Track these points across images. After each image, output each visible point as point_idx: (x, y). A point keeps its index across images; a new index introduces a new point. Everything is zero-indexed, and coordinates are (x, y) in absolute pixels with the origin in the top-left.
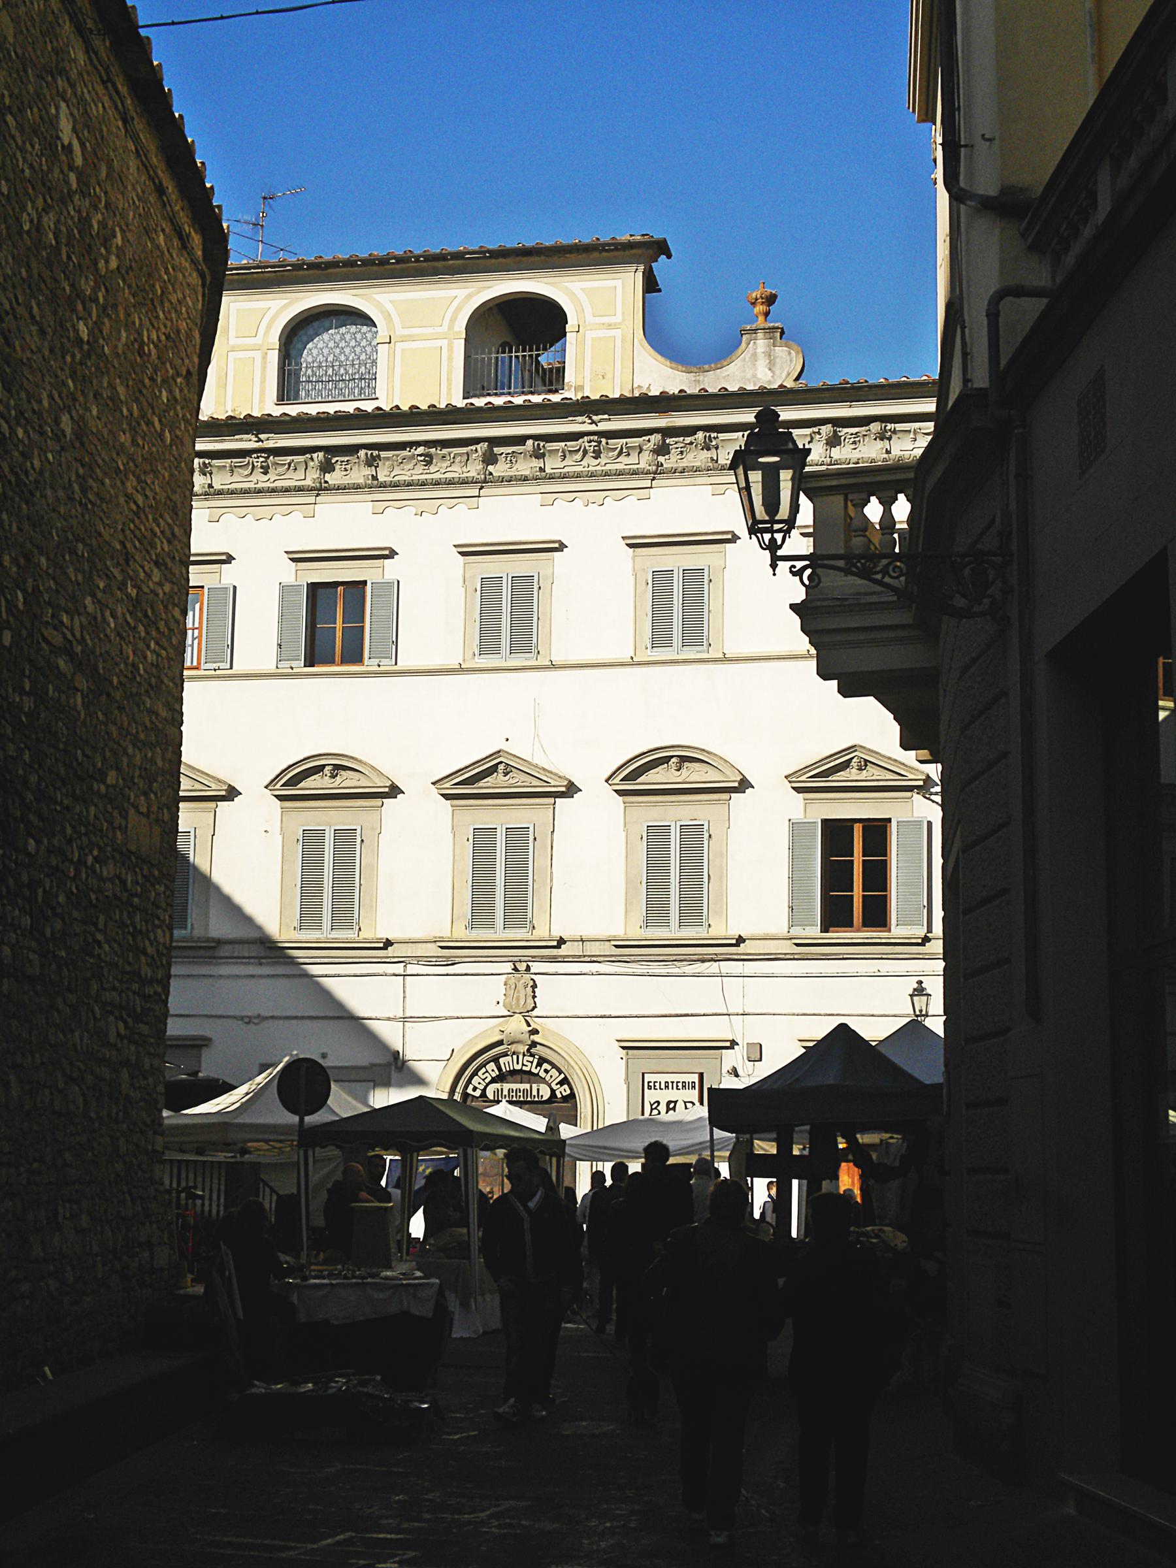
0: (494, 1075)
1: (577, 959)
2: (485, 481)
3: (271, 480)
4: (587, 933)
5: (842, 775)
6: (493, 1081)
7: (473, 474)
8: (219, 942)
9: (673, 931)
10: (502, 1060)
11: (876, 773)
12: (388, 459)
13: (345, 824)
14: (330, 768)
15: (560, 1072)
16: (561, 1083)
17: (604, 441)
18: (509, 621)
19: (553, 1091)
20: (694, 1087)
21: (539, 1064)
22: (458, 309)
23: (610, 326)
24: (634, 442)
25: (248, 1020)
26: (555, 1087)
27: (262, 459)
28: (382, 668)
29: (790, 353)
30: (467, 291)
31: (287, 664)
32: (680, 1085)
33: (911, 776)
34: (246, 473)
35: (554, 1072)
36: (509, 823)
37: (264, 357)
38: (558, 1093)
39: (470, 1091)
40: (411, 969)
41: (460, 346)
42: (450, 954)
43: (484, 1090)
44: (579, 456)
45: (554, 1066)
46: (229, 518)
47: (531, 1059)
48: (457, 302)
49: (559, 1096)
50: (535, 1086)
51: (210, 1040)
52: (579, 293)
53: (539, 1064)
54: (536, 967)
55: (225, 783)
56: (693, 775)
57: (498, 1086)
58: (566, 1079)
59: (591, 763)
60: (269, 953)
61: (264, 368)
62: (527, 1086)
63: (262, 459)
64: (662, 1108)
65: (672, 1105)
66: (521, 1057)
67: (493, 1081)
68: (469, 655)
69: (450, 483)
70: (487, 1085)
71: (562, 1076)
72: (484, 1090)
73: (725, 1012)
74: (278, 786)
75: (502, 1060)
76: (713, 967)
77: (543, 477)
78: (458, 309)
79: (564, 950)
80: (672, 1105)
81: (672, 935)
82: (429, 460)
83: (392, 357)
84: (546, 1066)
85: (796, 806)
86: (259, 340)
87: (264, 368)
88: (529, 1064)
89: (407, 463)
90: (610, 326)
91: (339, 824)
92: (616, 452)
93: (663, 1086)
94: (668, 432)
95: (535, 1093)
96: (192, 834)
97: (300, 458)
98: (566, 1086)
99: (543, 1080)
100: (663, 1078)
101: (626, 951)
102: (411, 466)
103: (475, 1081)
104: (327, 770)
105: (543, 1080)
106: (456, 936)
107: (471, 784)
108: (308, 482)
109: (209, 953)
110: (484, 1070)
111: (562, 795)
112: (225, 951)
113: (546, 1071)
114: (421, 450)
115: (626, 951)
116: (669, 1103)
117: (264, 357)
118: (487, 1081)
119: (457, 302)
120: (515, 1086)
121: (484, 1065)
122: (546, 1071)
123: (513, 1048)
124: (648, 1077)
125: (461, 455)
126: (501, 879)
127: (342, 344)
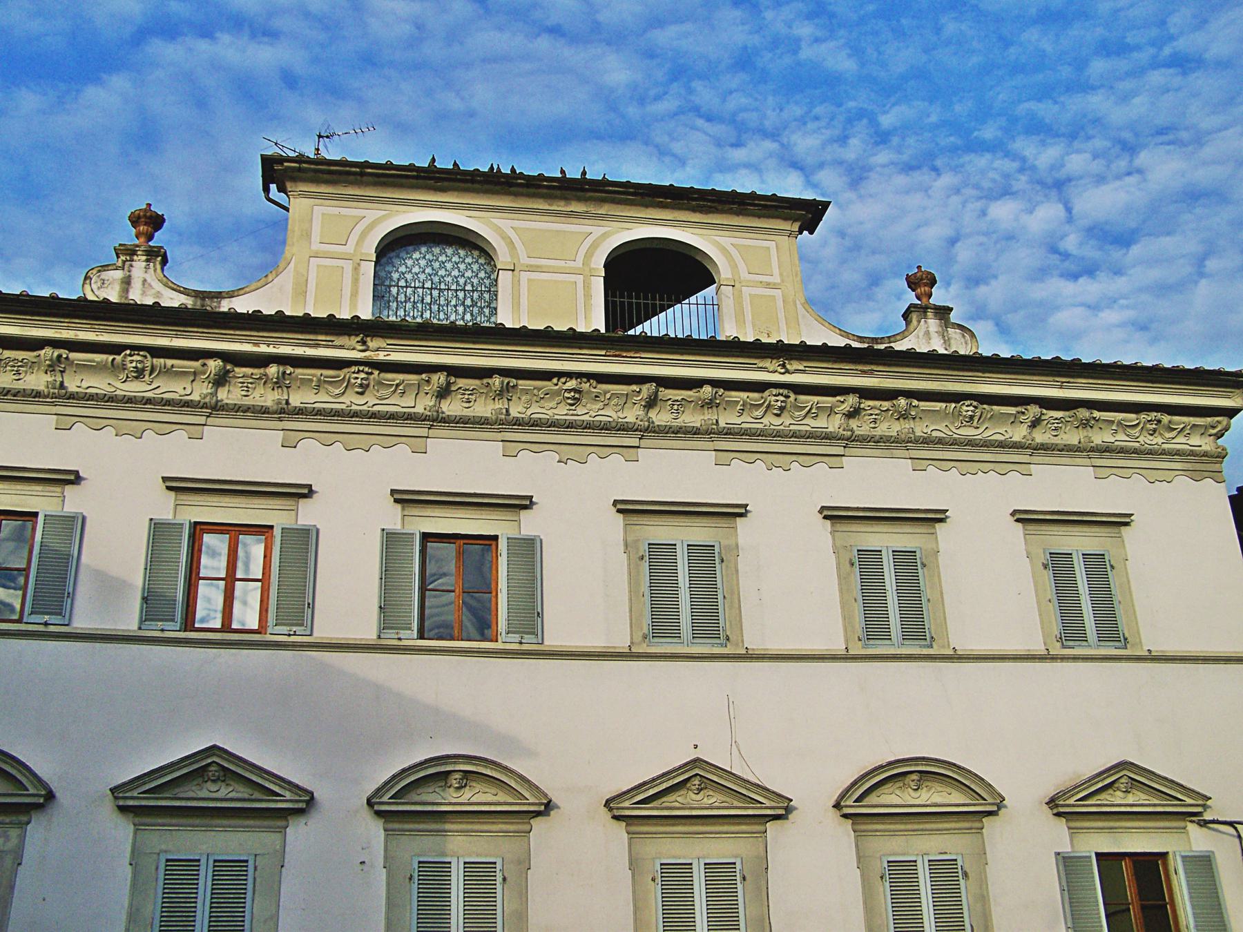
2: (646, 430)
3: (367, 402)
5: (1105, 797)
7: (631, 419)
11: (1143, 796)
12: (526, 392)
13: (674, 857)
14: (457, 776)
17: (793, 396)
23: (768, 285)
24: (828, 401)
27: (363, 375)
28: (525, 647)
30: (602, 230)
33: (1189, 801)
34: (337, 391)
37: (356, 269)
41: (599, 285)
44: (759, 413)
61: (356, 281)
63: (363, 375)
68: (638, 637)
69: (605, 428)
74: (385, 799)
77: (285, 412)
82: (577, 398)
83: (516, 284)
85: (1058, 836)
86: (350, 248)
87: (356, 281)
89: (552, 398)
90: (768, 285)
91: (470, 855)
96: (251, 863)
97: (413, 378)
102: (553, 404)
104: (454, 780)
108: (419, 409)
111: (538, 814)
114: (572, 384)
117: (356, 269)
125: (618, 396)
127: (442, 272)
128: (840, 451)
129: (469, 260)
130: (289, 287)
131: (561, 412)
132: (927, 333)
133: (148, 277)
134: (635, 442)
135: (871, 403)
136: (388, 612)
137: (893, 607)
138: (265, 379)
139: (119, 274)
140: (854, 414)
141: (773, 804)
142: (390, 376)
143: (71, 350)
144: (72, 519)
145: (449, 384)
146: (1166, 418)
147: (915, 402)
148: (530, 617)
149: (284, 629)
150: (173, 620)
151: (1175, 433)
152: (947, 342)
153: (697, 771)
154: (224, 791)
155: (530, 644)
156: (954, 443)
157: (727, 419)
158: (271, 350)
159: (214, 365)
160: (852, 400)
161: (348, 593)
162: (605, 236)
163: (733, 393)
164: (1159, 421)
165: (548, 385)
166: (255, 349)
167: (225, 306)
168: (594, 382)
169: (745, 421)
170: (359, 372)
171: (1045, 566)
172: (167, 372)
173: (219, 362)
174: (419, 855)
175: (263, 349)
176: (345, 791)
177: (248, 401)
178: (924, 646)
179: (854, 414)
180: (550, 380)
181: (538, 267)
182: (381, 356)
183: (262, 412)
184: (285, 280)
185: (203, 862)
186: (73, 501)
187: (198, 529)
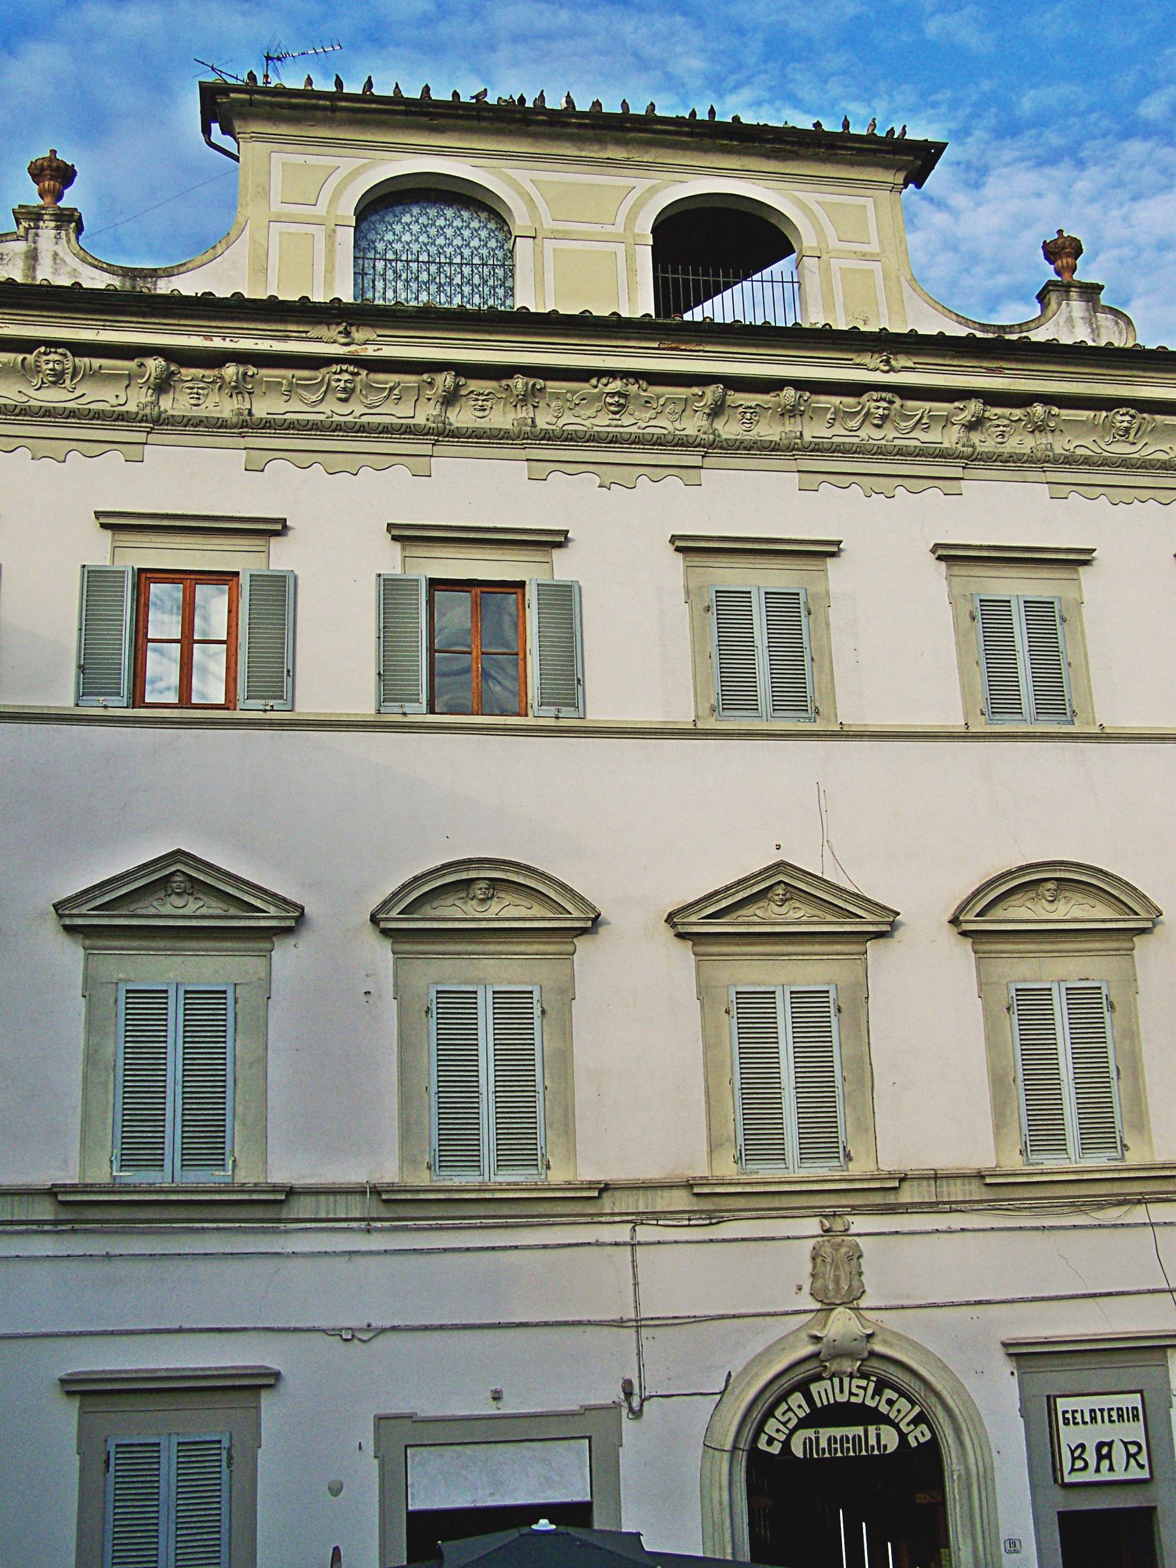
0: (802, 1414)
1: (932, 1207)
4: (943, 1161)
6: (803, 1424)
8: (291, 1192)
9: (1074, 1159)
10: (814, 1388)
12: (557, 396)
14: (483, 885)
15: (913, 1403)
16: (916, 1422)
17: (898, 402)
18: (764, 660)
19: (903, 1437)
20: (1136, 1417)
21: (878, 1392)
22: (638, 205)
23: (865, 257)
25: (348, 1336)
26: (905, 1429)
27: (346, 377)
29: (1117, 323)
30: (649, 183)
31: (393, 707)
32: (1114, 1414)
33: (869, 917)
34: (314, 398)
35: (903, 1404)
36: (793, 984)
37: (331, 236)
38: (911, 1439)
39: (762, 1445)
40: (645, 1233)
42: (710, 1202)
43: (786, 1444)
44: (855, 423)
45: (902, 1394)
46: (280, 468)
47: (863, 1383)
48: (635, 195)
49: (914, 1444)
50: (872, 1429)
51: (277, 1375)
52: (817, 209)
53: (878, 1392)
54: (860, 1224)
55: (594, 908)
56: (508, 910)
57: (810, 1433)
58: (921, 1413)
59: (924, 889)
60: (384, 1212)
62: (860, 1430)
63: (346, 377)
64: (1091, 1456)
65: (1105, 1451)
66: (846, 1380)
67: (803, 1424)
68: (705, 709)
69: (659, 442)
70: (792, 1431)
71: (917, 1409)
72: (786, 1444)
73: (1165, 1286)
74: (394, 914)
75: (814, 1388)
76: (1138, 1214)
77: (247, 425)
78: (638, 205)
79: (907, 1195)
80: (1105, 1451)
81: (1073, 1166)
82: (622, 404)
84: (889, 1394)
86: (321, 210)
88: (861, 1393)
90: (865, 257)
92: (912, 423)
93: (1087, 1418)
94: (992, 398)
95: (872, 1441)
96: (230, 995)
97: (411, 380)
98: (923, 1427)
99: (886, 1420)
100: (1085, 1404)
101: (997, 1191)
102: (591, 412)
103: (771, 1426)
105: (886, 1420)
106: (718, 1172)
107: (419, 917)
109: (270, 1213)
110: (784, 1407)
111: (583, 931)
112: (303, 1207)
113: (890, 1402)
114: (616, 385)
115: (997, 1191)
116: (1100, 1446)
117: (331, 236)
118: (791, 1425)
119: (635, 195)
120: (838, 1432)
121: (783, 1398)
122: (890, 1402)
123: (833, 1366)
124: (1062, 1404)
125: (674, 401)
126: (790, 1079)
127: (441, 241)
128: (958, 472)
130: (245, 263)
131: (602, 422)
132: (1070, 319)
133: (59, 249)
134: (696, 460)
135: (999, 411)
139: (21, 246)
140: (973, 426)
142: (381, 377)
145: (458, 387)
147: (1055, 410)
148: (567, 685)
149: (258, 703)
152: (1095, 331)
156: (1106, 463)
157: (815, 430)
158: (227, 344)
160: (974, 406)
161: (337, 658)
162: (653, 191)
163: (822, 398)
165: (584, 387)
166: (207, 344)
169: (838, 434)
170: (342, 371)
172: (94, 375)
173: (161, 362)
175: (217, 343)
179: (973, 426)
180: (587, 380)
181: (567, 232)
182: (370, 351)
183: (217, 426)
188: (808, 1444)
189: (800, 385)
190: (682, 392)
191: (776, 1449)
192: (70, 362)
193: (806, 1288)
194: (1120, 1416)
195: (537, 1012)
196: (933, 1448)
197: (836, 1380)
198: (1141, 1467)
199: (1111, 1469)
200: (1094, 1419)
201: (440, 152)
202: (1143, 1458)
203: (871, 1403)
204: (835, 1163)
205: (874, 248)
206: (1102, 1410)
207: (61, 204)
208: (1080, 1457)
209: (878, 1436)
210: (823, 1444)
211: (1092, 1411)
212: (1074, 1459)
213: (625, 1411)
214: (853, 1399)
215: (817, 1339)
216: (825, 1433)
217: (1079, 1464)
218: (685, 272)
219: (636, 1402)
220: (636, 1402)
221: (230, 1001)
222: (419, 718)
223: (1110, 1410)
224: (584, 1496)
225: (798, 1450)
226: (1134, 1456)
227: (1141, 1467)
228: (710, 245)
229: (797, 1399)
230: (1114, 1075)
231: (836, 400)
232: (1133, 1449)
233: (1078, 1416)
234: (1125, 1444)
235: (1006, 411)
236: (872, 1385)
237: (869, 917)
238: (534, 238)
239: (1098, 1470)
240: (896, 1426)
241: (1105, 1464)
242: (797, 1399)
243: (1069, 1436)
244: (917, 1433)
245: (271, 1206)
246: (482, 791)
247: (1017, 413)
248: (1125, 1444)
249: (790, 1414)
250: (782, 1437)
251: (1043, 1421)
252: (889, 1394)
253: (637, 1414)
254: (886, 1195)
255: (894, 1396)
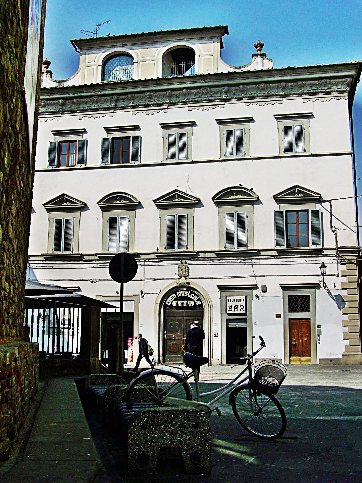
0: (175, 298)
6: (175, 300)
10: (177, 293)
19: (195, 303)
20: (244, 301)
21: (190, 294)
24: (219, 89)
31: (104, 163)
33: (194, 200)
35: (195, 297)
36: (179, 213)
37: (97, 68)
39: (167, 303)
43: (171, 303)
44: (200, 95)
47: (187, 292)
49: (197, 304)
50: (189, 301)
53: (190, 294)
57: (176, 301)
63: (96, 99)
64: (233, 308)
65: (236, 307)
67: (175, 300)
70: (173, 301)
71: (198, 298)
72: (171, 303)
73: (253, 275)
75: (177, 293)
80: (236, 307)
83: (138, 67)
84: (193, 294)
88: (187, 294)
93: (233, 301)
94: (229, 86)
95: (189, 304)
97: (108, 98)
98: (199, 301)
99: (192, 300)
100: (233, 298)
102: (145, 99)
105: (192, 300)
110: (171, 296)
113: (193, 296)
114: (148, 94)
115: (221, 255)
118: (172, 300)
122: (193, 296)
124: (228, 298)
128: (281, 99)
129: (129, 60)
130: (81, 76)
132: (257, 63)
133: (47, 79)
135: (232, 88)
136: (104, 159)
137: (235, 145)
138: (74, 103)
141: (195, 200)
142: (103, 98)
143: (247, 85)
144: (138, 137)
145: (117, 98)
146: (328, 81)
147: (245, 86)
148: (136, 157)
149: (79, 165)
150: (138, 160)
151: (332, 85)
153: (177, 192)
154: (242, 197)
155: (137, 163)
157: (192, 97)
158: (73, 95)
159: (115, 97)
160: (226, 88)
161: (94, 155)
163: (192, 90)
164: (326, 82)
165: (143, 95)
166: (69, 96)
167: (245, 70)
168: (154, 92)
170: (95, 98)
171: (283, 131)
172: (51, 104)
174: (110, 216)
175: (71, 95)
176: (207, 198)
177: (70, 109)
178: (243, 156)
179: (63, 105)
180: (143, 93)
181: (144, 60)
182: (99, 93)
183: (183, 103)
184: (79, 74)
185: (63, 220)
186: (138, 133)
187: (60, 142)
188: (176, 303)
189: (186, 88)
190: (162, 93)
191: (169, 304)
192: (46, 102)
193: (177, 274)
194: (240, 301)
195: (128, 221)
196: (201, 306)
197: (182, 292)
198: (244, 311)
199: (237, 311)
200: (234, 301)
201: (119, 46)
202: (244, 309)
203: (189, 296)
204: (185, 249)
205: (212, 53)
206: (236, 299)
207: (48, 69)
208: (231, 308)
209: (190, 303)
210: (179, 304)
211: (234, 299)
212: (229, 309)
213: (141, 296)
214: (185, 295)
215: (178, 283)
216: (179, 302)
217: (230, 310)
218: (190, 63)
219: (143, 295)
220: (143, 295)
221: (73, 221)
222: (108, 165)
223: (238, 299)
224: (133, 311)
225: (173, 304)
226: (242, 308)
227: (244, 311)
228: (181, 58)
229: (174, 295)
230: (246, 231)
231: (195, 90)
232: (242, 307)
233: (231, 300)
234: (241, 306)
235: (234, 88)
236: (189, 293)
237: (194, 200)
238: (137, 62)
239: (234, 311)
240: (194, 301)
241: (236, 310)
242: (174, 295)
243: (229, 304)
244: (198, 302)
245: (80, 257)
246: (119, 180)
247: (237, 88)
248: (241, 306)
249: (172, 298)
250: (171, 302)
251: (224, 301)
252: (193, 294)
253: (143, 297)
254: (195, 256)
255: (194, 295)
